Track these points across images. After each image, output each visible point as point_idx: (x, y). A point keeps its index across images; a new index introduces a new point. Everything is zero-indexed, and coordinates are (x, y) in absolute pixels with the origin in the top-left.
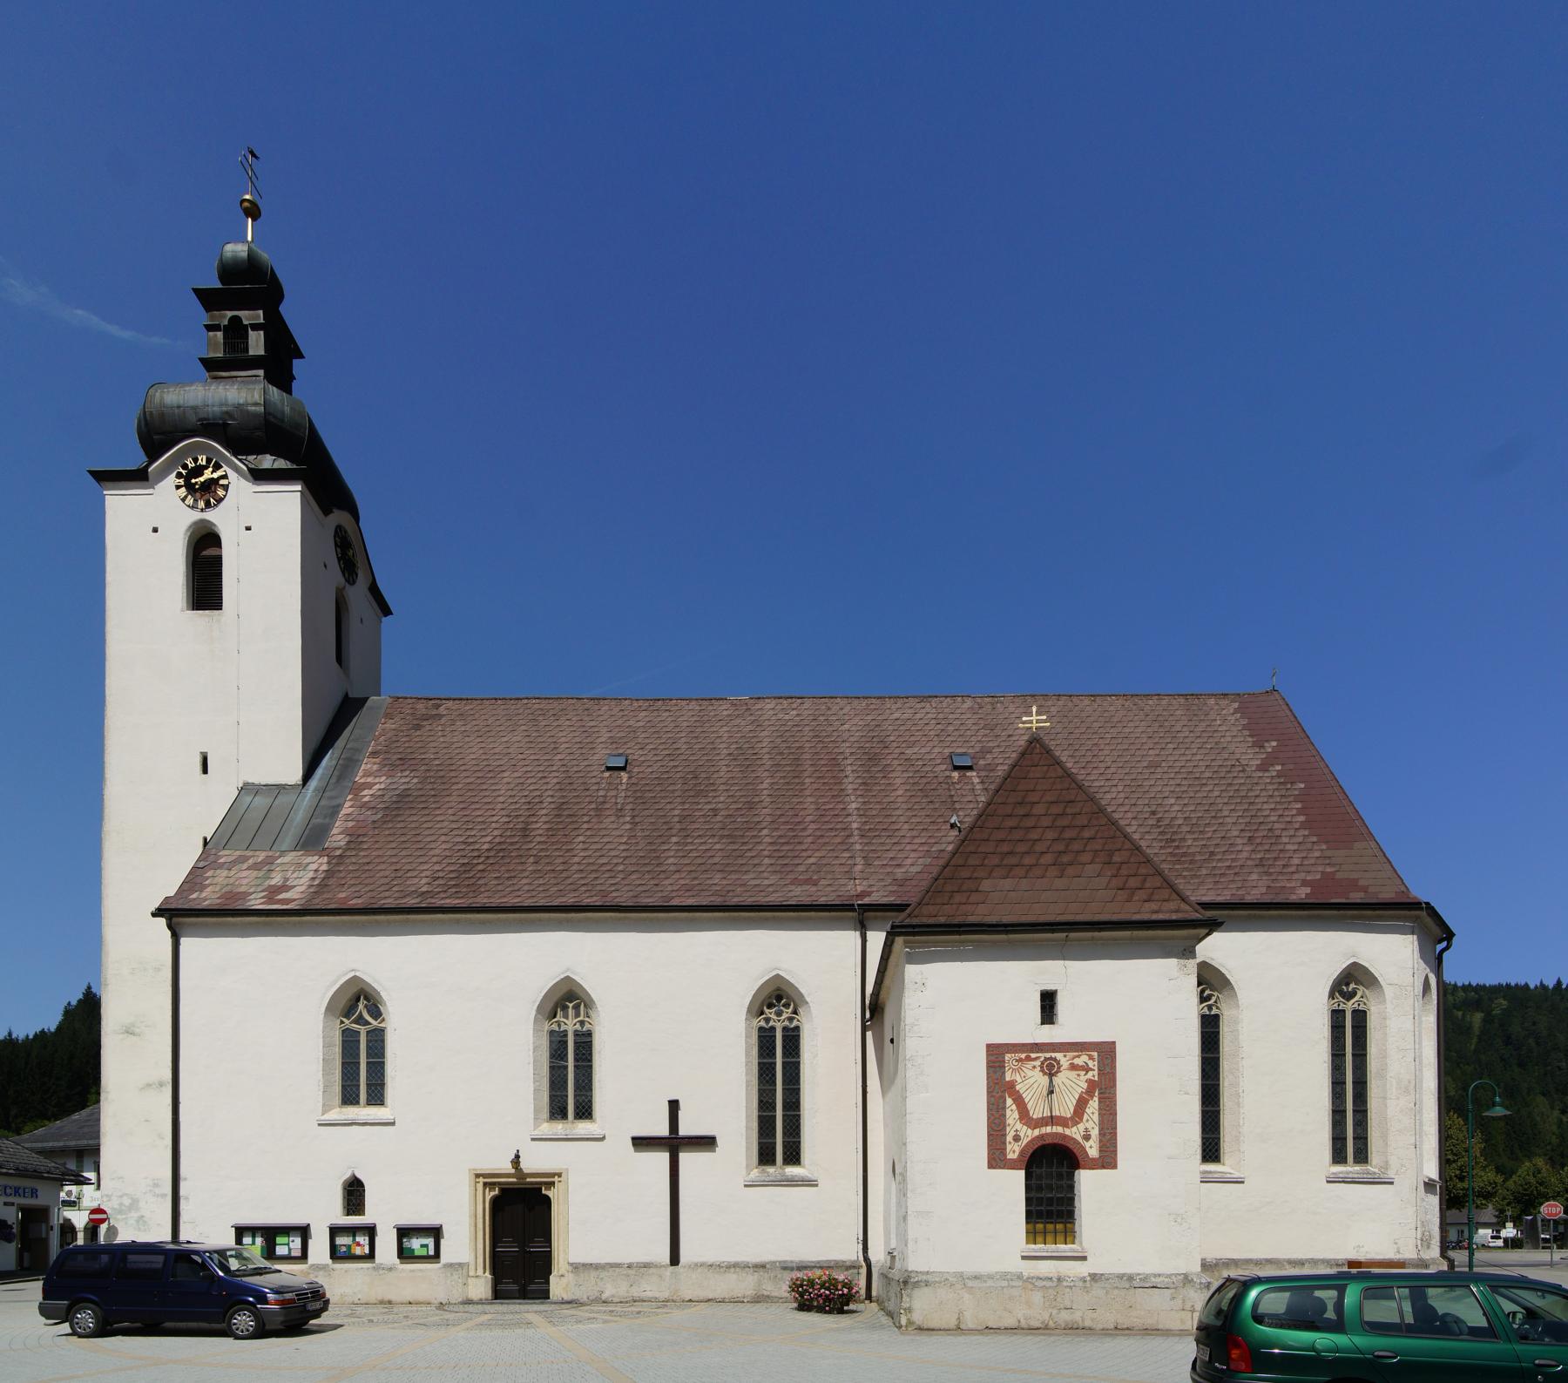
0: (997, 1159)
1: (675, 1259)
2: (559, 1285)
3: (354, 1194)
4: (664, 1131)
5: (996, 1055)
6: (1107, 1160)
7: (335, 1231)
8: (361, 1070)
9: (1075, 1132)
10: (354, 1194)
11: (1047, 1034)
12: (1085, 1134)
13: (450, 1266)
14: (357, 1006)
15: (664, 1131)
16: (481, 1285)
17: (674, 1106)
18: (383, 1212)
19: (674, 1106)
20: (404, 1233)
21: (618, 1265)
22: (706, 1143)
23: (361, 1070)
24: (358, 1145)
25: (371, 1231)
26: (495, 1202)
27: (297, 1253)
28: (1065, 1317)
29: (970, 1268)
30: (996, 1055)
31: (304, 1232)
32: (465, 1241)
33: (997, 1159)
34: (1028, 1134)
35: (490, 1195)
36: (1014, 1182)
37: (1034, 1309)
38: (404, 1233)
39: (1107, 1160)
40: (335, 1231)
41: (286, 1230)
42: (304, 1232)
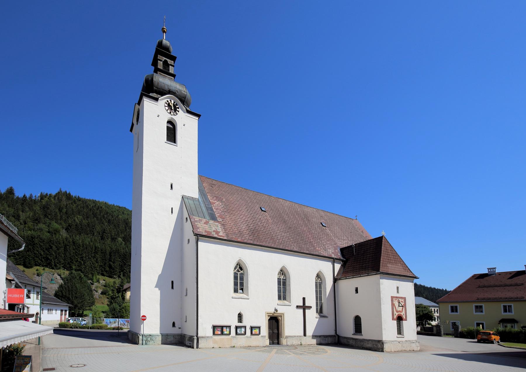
0: (393, 319)
1: (305, 335)
2: (283, 341)
3: (240, 316)
4: (302, 305)
5: (392, 298)
6: (406, 320)
7: (237, 328)
8: (240, 283)
9: (402, 314)
10: (240, 316)
11: (398, 295)
12: (403, 314)
13: (262, 336)
14: (398, 292)
15: (302, 305)
16: (267, 342)
17: (304, 299)
18: (247, 322)
19: (304, 299)
20: (252, 328)
21: (295, 336)
22: (310, 307)
23: (240, 283)
24: (240, 303)
25: (245, 327)
26: (269, 320)
27: (243, 333)
28: (404, 349)
29: (410, 340)
30: (392, 298)
31: (230, 327)
32: (265, 331)
33: (393, 319)
34: (397, 314)
35: (268, 318)
36: (395, 322)
37: (399, 347)
38: (252, 328)
39: (406, 320)
40: (237, 328)
41: (226, 327)
42: (230, 327)
